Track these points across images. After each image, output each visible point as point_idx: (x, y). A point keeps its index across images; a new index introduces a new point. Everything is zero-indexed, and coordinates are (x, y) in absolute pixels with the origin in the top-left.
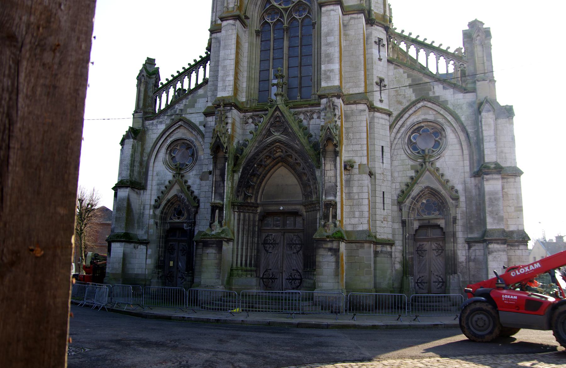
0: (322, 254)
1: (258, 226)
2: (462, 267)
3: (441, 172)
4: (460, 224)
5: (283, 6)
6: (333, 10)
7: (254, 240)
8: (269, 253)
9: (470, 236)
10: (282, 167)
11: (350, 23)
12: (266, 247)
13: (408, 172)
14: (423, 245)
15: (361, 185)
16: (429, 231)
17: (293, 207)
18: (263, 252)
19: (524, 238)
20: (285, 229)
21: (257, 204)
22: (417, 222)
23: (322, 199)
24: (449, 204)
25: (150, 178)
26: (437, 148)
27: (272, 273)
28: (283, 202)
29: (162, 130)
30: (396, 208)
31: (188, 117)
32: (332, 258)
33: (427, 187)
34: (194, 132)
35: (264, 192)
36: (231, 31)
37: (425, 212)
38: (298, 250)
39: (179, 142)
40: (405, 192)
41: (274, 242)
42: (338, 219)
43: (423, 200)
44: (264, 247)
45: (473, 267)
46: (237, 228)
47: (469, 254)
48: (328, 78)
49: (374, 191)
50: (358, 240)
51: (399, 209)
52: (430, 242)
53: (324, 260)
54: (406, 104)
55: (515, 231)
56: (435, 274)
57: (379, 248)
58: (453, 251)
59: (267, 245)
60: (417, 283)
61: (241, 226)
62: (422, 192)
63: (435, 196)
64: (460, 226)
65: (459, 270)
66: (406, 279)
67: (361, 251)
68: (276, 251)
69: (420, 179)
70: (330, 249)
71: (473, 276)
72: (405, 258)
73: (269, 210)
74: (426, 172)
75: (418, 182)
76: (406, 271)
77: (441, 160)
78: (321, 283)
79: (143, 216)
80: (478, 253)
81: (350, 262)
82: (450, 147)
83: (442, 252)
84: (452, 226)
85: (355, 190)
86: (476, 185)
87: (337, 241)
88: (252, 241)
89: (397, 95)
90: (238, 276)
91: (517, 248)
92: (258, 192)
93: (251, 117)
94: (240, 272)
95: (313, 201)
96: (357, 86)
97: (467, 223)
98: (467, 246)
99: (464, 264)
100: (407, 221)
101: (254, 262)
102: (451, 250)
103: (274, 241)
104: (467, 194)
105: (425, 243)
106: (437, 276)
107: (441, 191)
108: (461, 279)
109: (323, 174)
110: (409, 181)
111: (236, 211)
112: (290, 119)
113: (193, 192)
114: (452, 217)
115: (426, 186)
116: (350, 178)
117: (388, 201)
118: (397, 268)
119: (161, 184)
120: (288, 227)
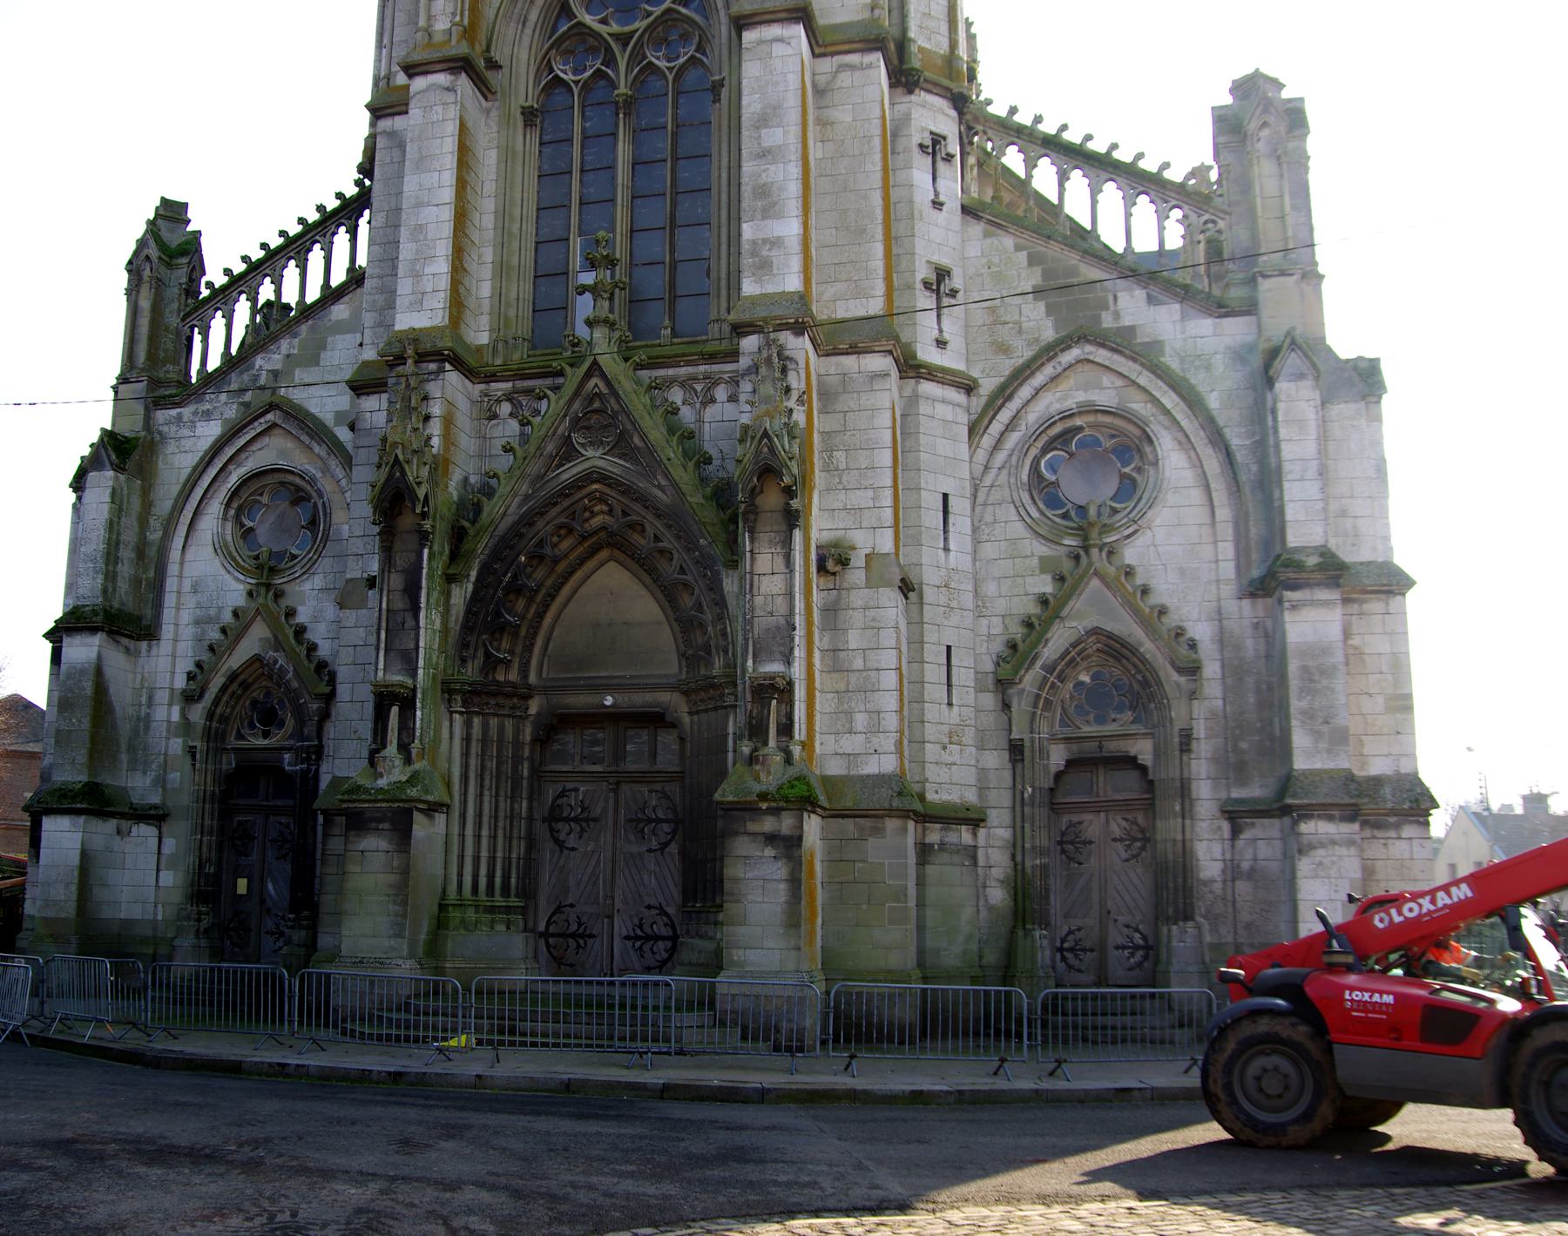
0: (745, 854)
1: (531, 760)
3: (1139, 581)
5: (615, 28)
6: (780, 40)
7: (516, 806)
8: (566, 852)
9: (1236, 793)
10: (612, 564)
11: (838, 83)
12: (558, 832)
13: (1029, 580)
14: (1080, 823)
15: (873, 624)
17: (649, 697)
19: (1417, 801)
23: (744, 671)
25: (170, 600)
26: (1128, 499)
28: (615, 681)
29: (211, 440)
30: (989, 700)
31: (298, 396)
34: (317, 449)
36: (439, 109)
37: (1088, 713)
38: (663, 840)
39: (269, 479)
40: (1021, 647)
41: (585, 815)
42: (797, 737)
43: (1079, 673)
44: (552, 830)
45: (1249, 898)
47: (1233, 853)
48: (765, 266)
51: (1000, 704)
52: (1102, 814)
53: (749, 875)
54: (1024, 353)
55: (1388, 777)
57: (934, 835)
58: (1180, 845)
59: (560, 826)
60: (1061, 950)
63: (1119, 661)
65: (1201, 907)
67: (872, 841)
69: (1071, 603)
70: (771, 839)
71: (1248, 926)
72: (1019, 867)
74: (1090, 580)
75: (1064, 613)
76: (1024, 910)
77: (1140, 541)
78: (741, 952)
79: (147, 728)
80: (1264, 850)
81: (837, 880)
82: (1171, 498)
83: (1143, 848)
84: (1177, 762)
85: (854, 639)
88: (512, 810)
89: (995, 323)
91: (1392, 834)
92: (529, 649)
93: (509, 397)
94: (471, 914)
95: (715, 677)
96: (862, 294)
98: (1226, 826)
99: (1217, 887)
100: (1027, 743)
102: (1174, 840)
103: (583, 810)
104: (1225, 653)
105: (1088, 817)
106: (1127, 926)
108: (1208, 939)
109: (748, 588)
110: (1033, 609)
111: (456, 712)
112: (638, 403)
113: (312, 648)
114: (1176, 729)
116: (838, 600)
117: (963, 676)
118: (992, 902)
119: (209, 620)
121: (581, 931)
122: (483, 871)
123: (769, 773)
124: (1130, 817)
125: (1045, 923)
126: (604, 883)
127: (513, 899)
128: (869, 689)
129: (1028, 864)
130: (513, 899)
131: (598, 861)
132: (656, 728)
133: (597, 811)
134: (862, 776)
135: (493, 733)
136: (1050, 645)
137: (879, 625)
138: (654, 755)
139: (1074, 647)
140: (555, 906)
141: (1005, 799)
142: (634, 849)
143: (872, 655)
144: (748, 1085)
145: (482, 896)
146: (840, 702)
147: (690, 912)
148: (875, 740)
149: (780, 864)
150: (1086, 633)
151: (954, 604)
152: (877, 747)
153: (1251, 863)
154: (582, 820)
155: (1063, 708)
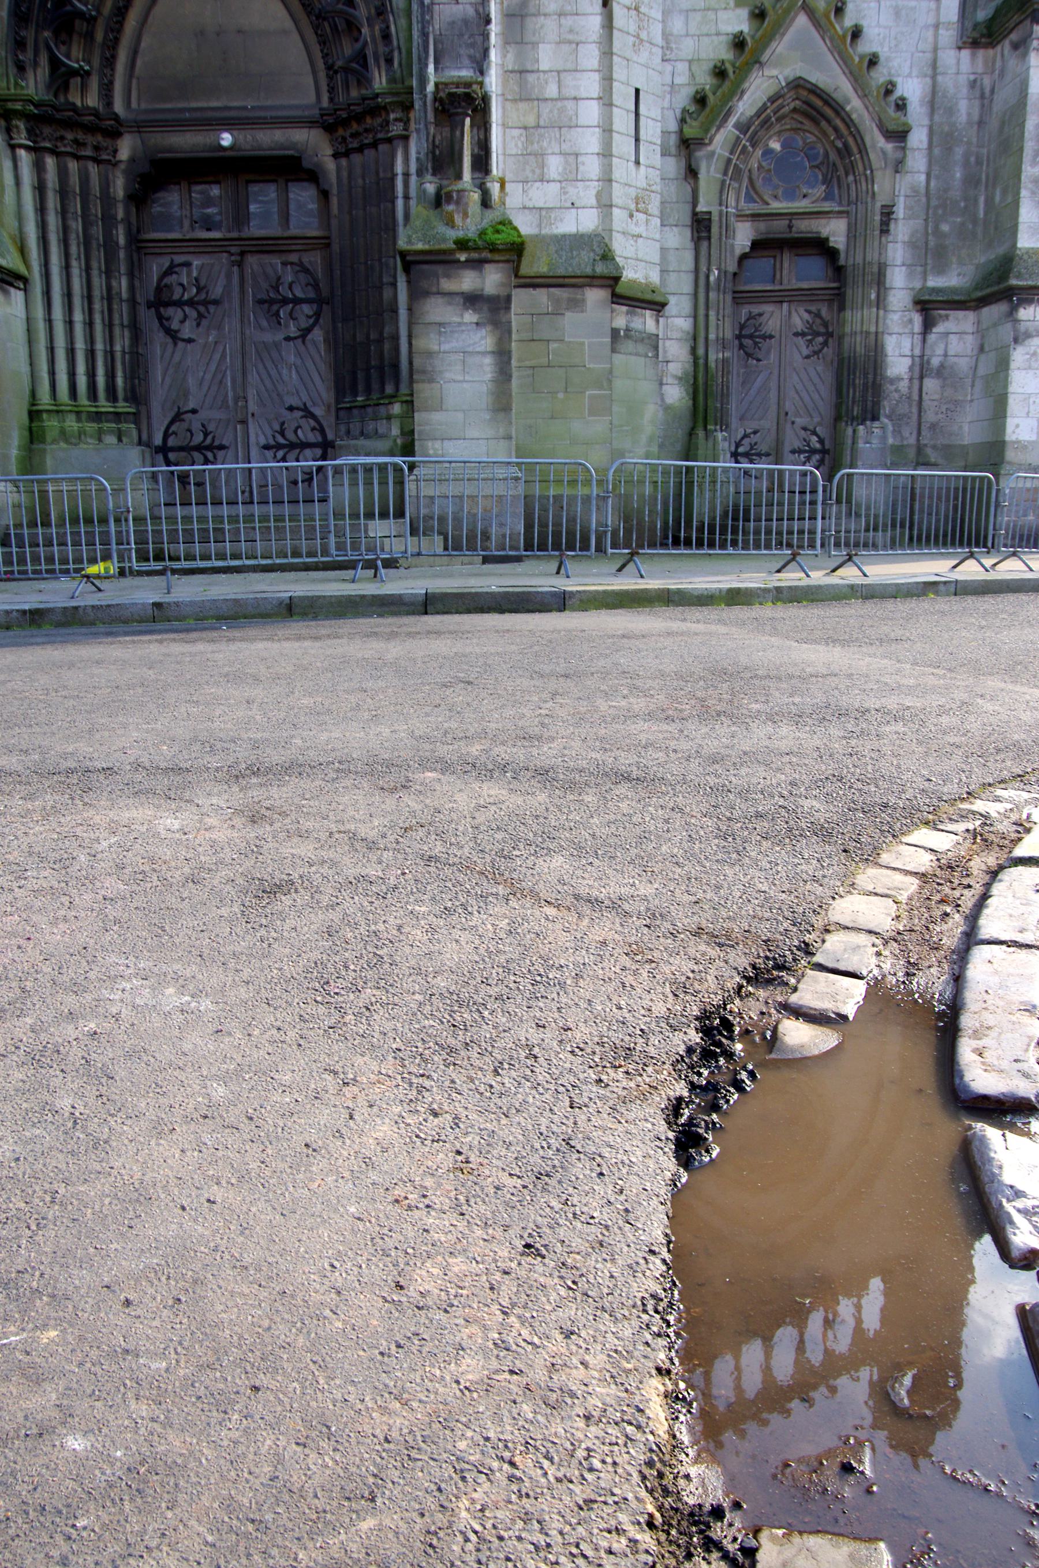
0: (438, 319)
1: (127, 220)
2: (896, 396)
4: (900, 237)
7: (114, 283)
8: (181, 344)
9: (931, 283)
12: (168, 319)
13: (723, 15)
14: (760, 315)
15: (571, 37)
16: (786, 265)
18: (158, 340)
20: (244, 235)
21: (116, 118)
22: (748, 225)
23: (423, 80)
24: (872, 156)
27: (203, 426)
28: (233, 114)
30: (673, 166)
32: (482, 338)
33: (798, 84)
35: (139, 63)
37: (777, 187)
38: (304, 325)
40: (711, 99)
41: (203, 296)
42: (494, 171)
43: (770, 138)
44: (160, 318)
45: (936, 397)
46: (37, 226)
47: (923, 348)
49: (608, 79)
50: (561, 271)
51: (683, 171)
52: (785, 305)
53: (445, 347)
56: (800, 421)
58: (872, 337)
59: (170, 311)
61: (53, 221)
62: (776, 105)
63: (816, 123)
64: (899, 246)
65: (886, 407)
66: (707, 438)
68: (214, 332)
69: (774, 44)
70: (472, 300)
71: (933, 427)
72: (701, 361)
73: (170, 150)
74: (796, 15)
75: (764, 58)
76: (706, 410)
78: (438, 445)
80: (955, 345)
81: (528, 363)
83: (825, 344)
84: (876, 243)
85: (546, 57)
86: (975, 81)
87: (501, 265)
88: (109, 288)
90: (67, 441)
92: (110, 62)
94: (71, 423)
95: (377, 95)
97: (927, 234)
98: (917, 319)
99: (903, 386)
100: (715, 217)
101: (125, 383)
102: (868, 333)
103: (199, 290)
104: (936, 118)
105: (768, 308)
106: (805, 429)
107: (848, 102)
108: (890, 441)
110: (726, 54)
111: (21, 146)
114: (878, 205)
115: (791, 78)
118: (669, 401)
120: (255, 230)
121: (208, 441)
122: (81, 368)
123: (466, 215)
124: (813, 308)
125: (725, 425)
126: (234, 381)
127: (121, 403)
128: (565, 125)
129: (712, 357)
130: (121, 403)
131: (223, 355)
132: (287, 181)
133: (217, 292)
134: (556, 236)
135: (74, 180)
136: (745, 97)
137: (577, 38)
138: (285, 217)
139: (773, 103)
140: (173, 414)
141: (686, 284)
142: (268, 337)
143: (568, 79)
144: (540, 589)
145: (83, 400)
146: (529, 140)
147: (350, 408)
148: (572, 191)
149: (483, 332)
150: (788, 84)
151: (644, 35)
152: (574, 199)
153: (940, 359)
154: (198, 303)
155: (751, 180)
